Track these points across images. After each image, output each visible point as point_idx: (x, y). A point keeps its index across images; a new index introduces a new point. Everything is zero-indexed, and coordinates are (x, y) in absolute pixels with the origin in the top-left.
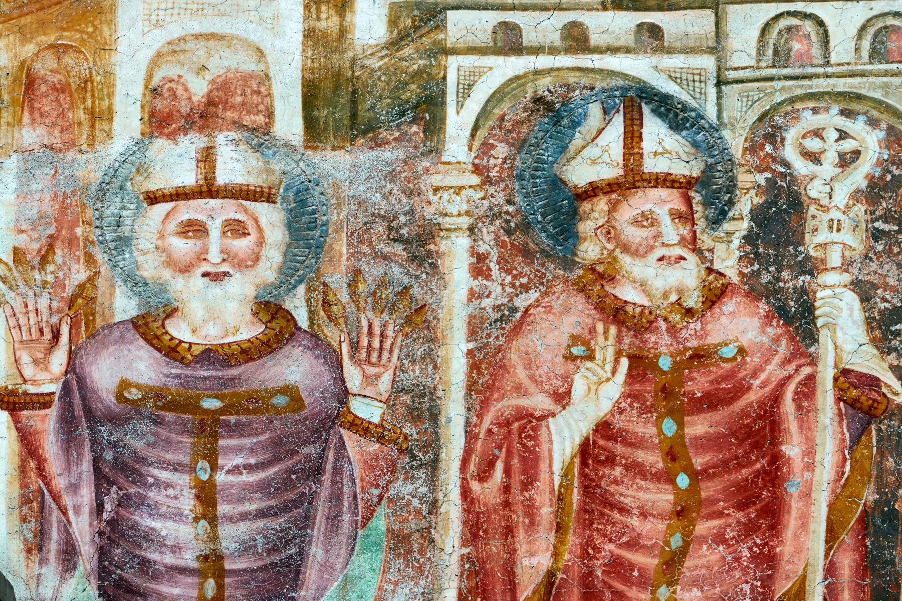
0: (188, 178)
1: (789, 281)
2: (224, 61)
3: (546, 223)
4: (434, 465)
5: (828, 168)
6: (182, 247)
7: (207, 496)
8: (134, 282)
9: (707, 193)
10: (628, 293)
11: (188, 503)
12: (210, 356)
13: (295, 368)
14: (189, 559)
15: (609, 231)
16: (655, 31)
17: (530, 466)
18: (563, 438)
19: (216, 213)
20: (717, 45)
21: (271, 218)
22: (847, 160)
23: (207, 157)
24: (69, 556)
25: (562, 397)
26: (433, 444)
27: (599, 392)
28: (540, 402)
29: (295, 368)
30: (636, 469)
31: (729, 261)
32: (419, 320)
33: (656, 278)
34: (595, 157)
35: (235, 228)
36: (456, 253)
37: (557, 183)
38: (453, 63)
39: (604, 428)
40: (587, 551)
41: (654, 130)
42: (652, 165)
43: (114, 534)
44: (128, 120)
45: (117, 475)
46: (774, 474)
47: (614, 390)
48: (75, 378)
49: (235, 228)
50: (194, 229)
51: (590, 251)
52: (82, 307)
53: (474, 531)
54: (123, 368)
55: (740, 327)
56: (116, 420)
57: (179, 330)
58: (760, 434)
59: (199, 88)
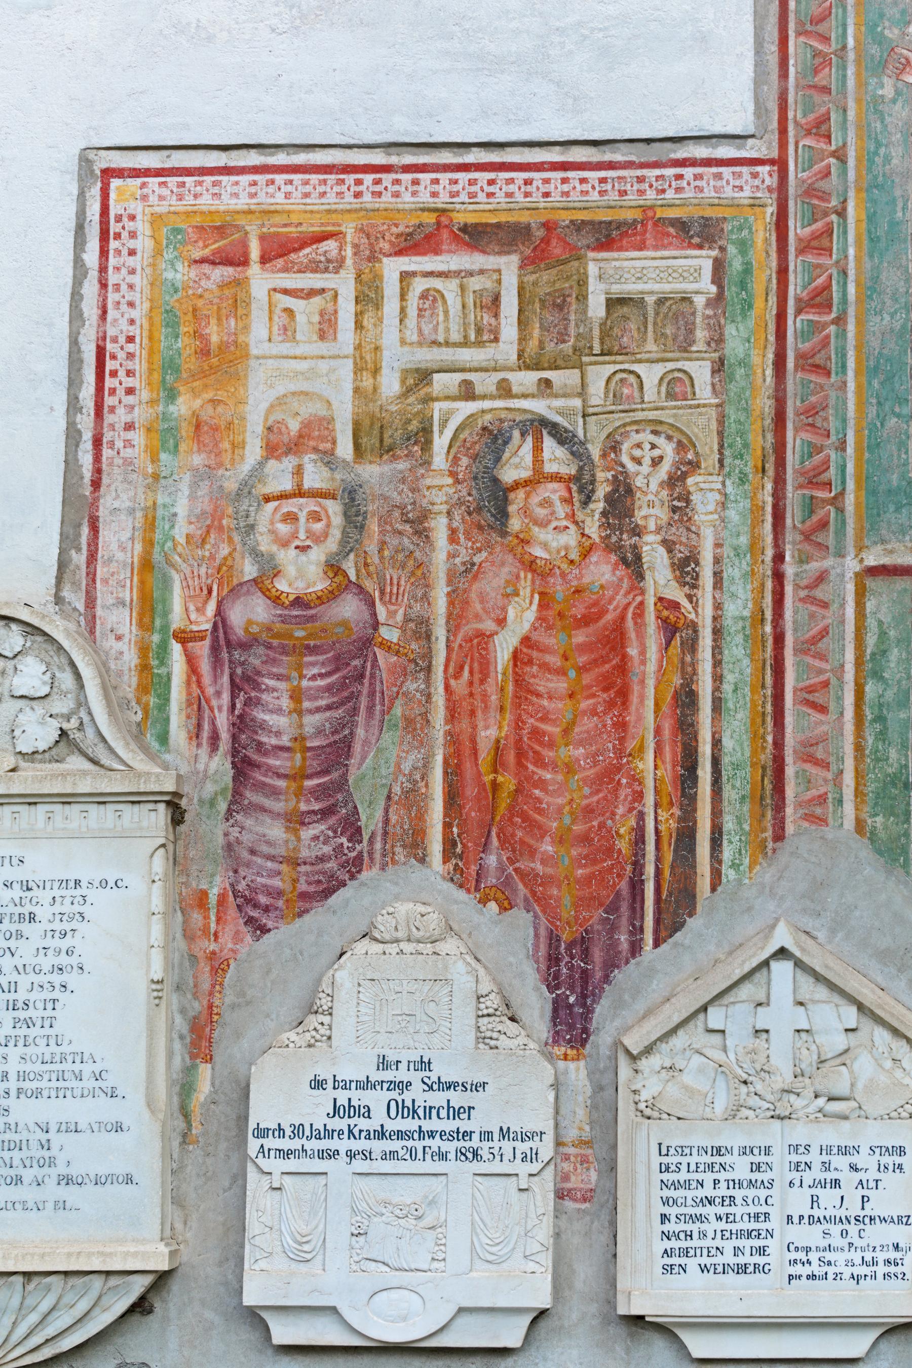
0: (287, 485)
1: (628, 540)
2: (309, 409)
3: (491, 504)
4: (429, 669)
5: (645, 468)
6: (284, 529)
7: (296, 696)
8: (256, 554)
9: (581, 485)
10: (538, 552)
11: (285, 703)
12: (298, 602)
13: (348, 608)
14: (285, 741)
15: (525, 511)
16: (548, 383)
17: (484, 668)
18: (503, 648)
19: (303, 507)
20: (582, 392)
21: (334, 508)
22: (656, 462)
23: (299, 471)
24: (215, 738)
25: (501, 622)
26: (428, 655)
27: (522, 617)
28: (489, 625)
29: (348, 608)
30: (545, 667)
31: (593, 529)
32: (421, 574)
33: (553, 541)
34: (515, 466)
35: (315, 517)
36: (440, 528)
37: (496, 481)
38: (437, 406)
39: (526, 640)
40: (518, 724)
41: (549, 443)
42: (550, 468)
43: (242, 724)
44: (254, 451)
45: (244, 684)
46: (623, 668)
47: (531, 615)
48: (221, 619)
49: (315, 517)
50: (291, 518)
51: (515, 524)
52: (224, 570)
53: (452, 714)
54: (251, 613)
55: (602, 572)
56: (245, 646)
57: (282, 585)
58: (615, 641)
59: (294, 426)
